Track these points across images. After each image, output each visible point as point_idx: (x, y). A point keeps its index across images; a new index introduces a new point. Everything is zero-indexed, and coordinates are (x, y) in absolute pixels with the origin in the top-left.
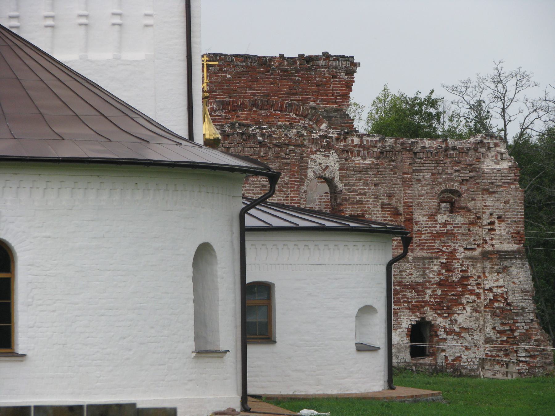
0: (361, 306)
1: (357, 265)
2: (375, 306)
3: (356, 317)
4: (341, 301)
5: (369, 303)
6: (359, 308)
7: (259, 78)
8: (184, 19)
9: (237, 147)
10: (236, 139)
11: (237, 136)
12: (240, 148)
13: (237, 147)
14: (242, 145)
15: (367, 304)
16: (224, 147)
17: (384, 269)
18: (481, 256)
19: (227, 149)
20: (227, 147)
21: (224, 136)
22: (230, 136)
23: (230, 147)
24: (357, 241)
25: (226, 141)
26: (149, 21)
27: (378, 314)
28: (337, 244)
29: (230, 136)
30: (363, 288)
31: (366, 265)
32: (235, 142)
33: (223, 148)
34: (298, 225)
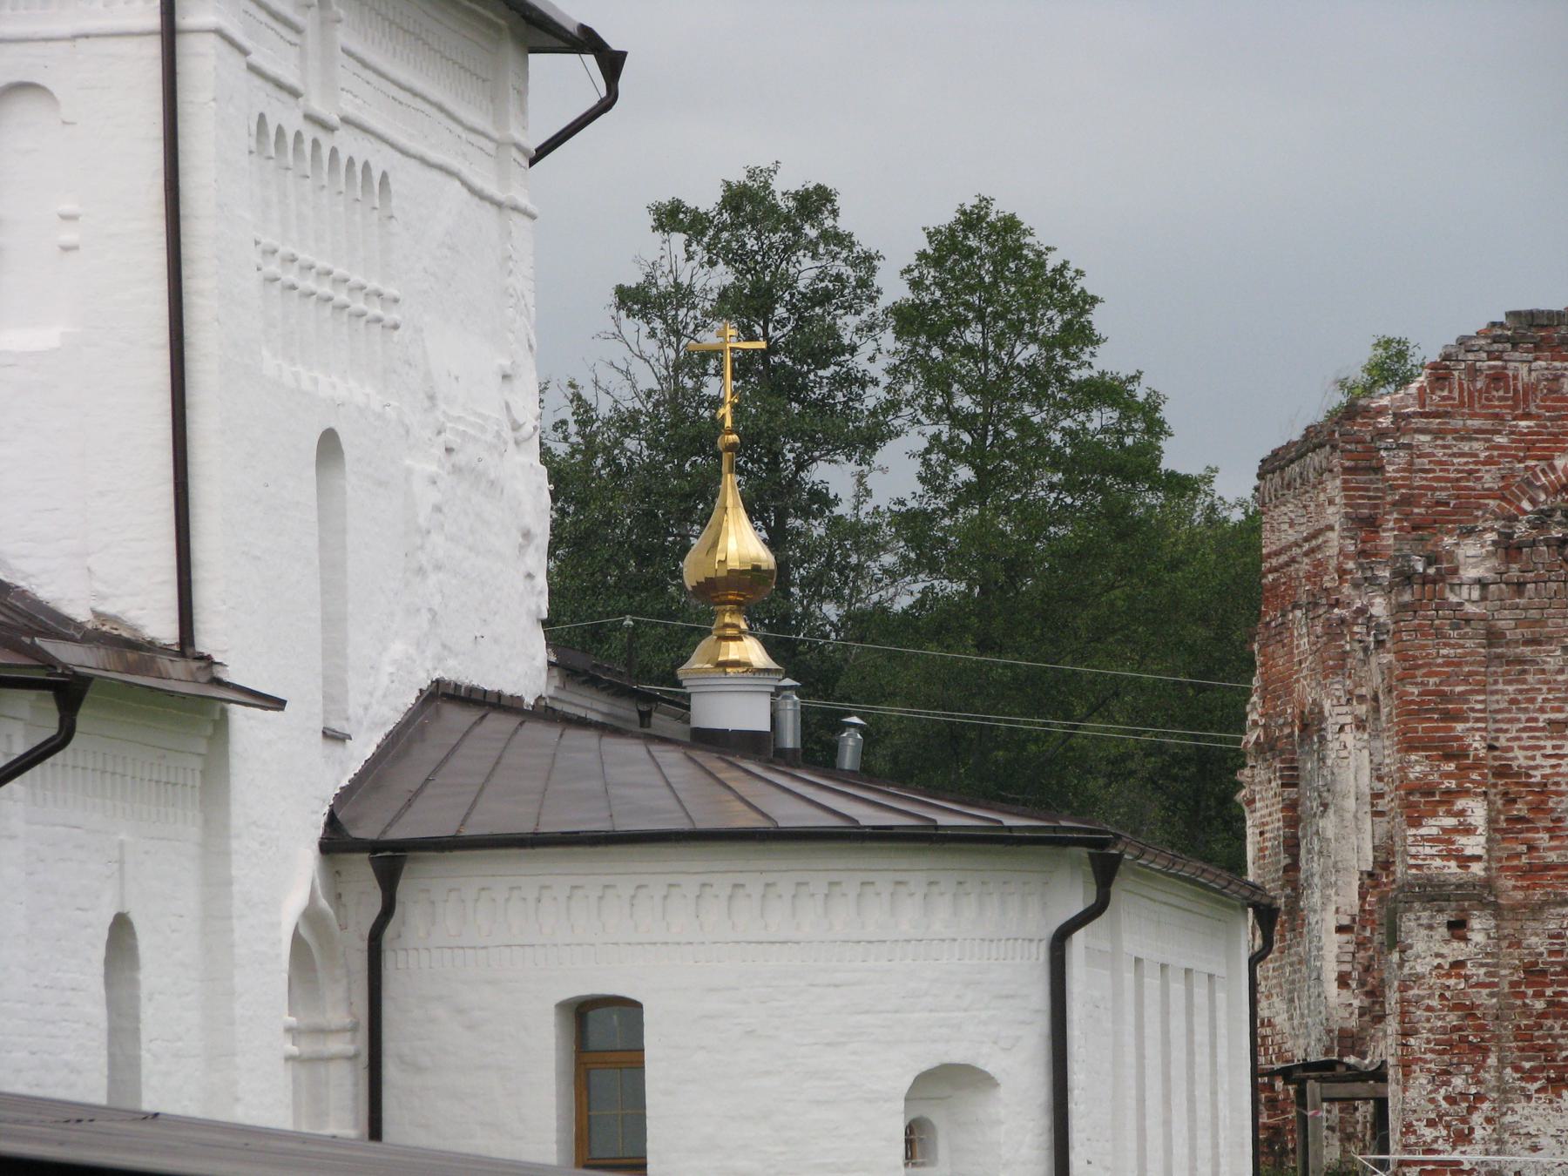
0: (925, 1066)
1: (908, 941)
2: (990, 1063)
3: (906, 1099)
4: (854, 1053)
5: (957, 1055)
6: (917, 1073)
7: (1067, 382)
8: (160, 226)
9: (1545, 582)
10: (1544, 559)
11: (1545, 548)
12: (1554, 586)
13: (1545, 582)
14: (1561, 575)
15: (947, 1060)
16: (1507, 584)
17: (1041, 954)
18: (1247, 912)
19: (1515, 587)
20: (1513, 583)
21: (1506, 548)
22: (1524, 550)
23: (1525, 583)
24: (877, 870)
25: (1514, 566)
26: (69, 236)
27: (1002, 1092)
28: (837, 880)
29: (1524, 550)
30: (931, 1011)
31: (943, 940)
32: (1541, 566)
33: (1503, 586)
34: (857, 822)
